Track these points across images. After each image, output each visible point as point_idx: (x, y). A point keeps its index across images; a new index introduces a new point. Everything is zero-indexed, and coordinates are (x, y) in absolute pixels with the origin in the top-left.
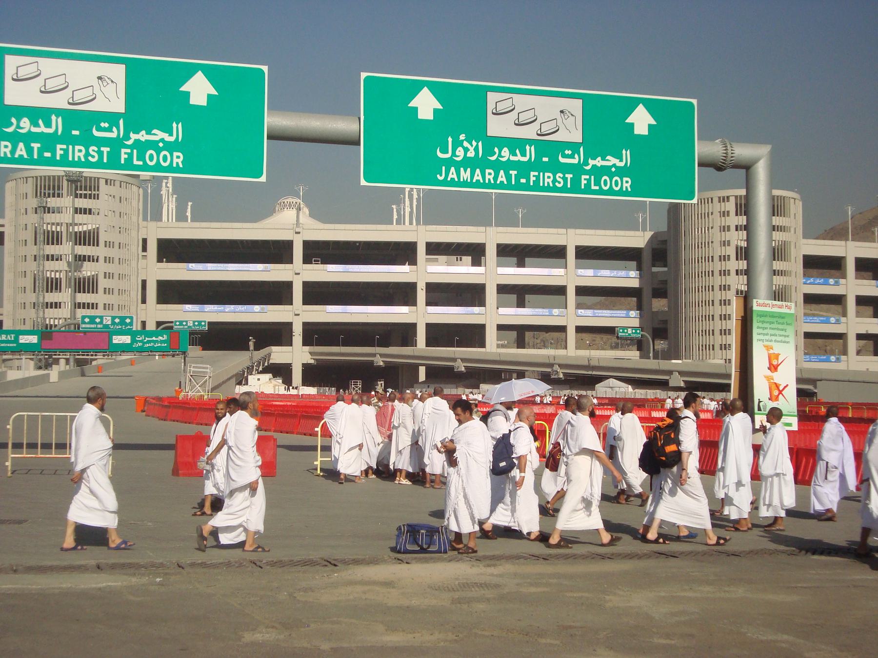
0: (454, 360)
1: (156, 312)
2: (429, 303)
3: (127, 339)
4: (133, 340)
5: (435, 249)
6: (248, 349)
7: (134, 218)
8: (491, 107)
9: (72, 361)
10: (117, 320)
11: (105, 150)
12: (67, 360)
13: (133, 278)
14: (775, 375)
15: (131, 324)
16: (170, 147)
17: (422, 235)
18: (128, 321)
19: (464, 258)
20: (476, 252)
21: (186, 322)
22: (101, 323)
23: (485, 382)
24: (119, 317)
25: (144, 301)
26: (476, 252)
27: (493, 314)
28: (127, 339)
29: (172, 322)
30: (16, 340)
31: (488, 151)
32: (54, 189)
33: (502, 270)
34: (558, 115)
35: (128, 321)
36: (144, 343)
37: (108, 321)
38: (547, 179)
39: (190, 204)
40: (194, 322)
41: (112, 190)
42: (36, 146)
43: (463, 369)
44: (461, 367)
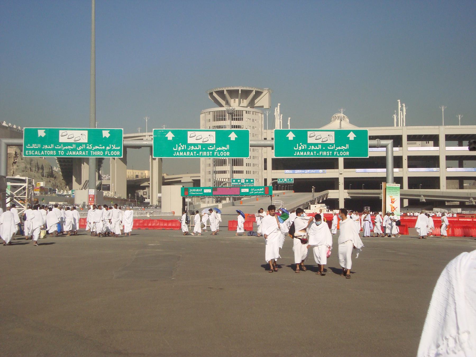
0: (420, 196)
1: (272, 174)
2: (409, 167)
3: (247, 190)
4: (250, 191)
5: (412, 138)
6: (311, 191)
7: (260, 129)
8: (308, 135)
9: (231, 198)
10: (247, 181)
11: (211, 152)
12: (230, 198)
13: (260, 158)
14: (393, 204)
15: (253, 182)
16: (226, 151)
17: (404, 131)
18: (252, 181)
19: (430, 142)
20: (434, 139)
21: (240, 180)
22: (240, 182)
23: (436, 207)
24: (248, 180)
25: (265, 169)
26: (434, 139)
27: (443, 172)
28: (247, 190)
29: (277, 179)
30: (203, 191)
31: (308, 147)
32: (222, 116)
33: (448, 148)
34: (327, 136)
35: (252, 181)
36: (254, 192)
37: (243, 181)
38: (325, 153)
39: (289, 118)
40: (287, 179)
41: (250, 116)
42: (195, 152)
43: (424, 200)
44: (423, 199)
